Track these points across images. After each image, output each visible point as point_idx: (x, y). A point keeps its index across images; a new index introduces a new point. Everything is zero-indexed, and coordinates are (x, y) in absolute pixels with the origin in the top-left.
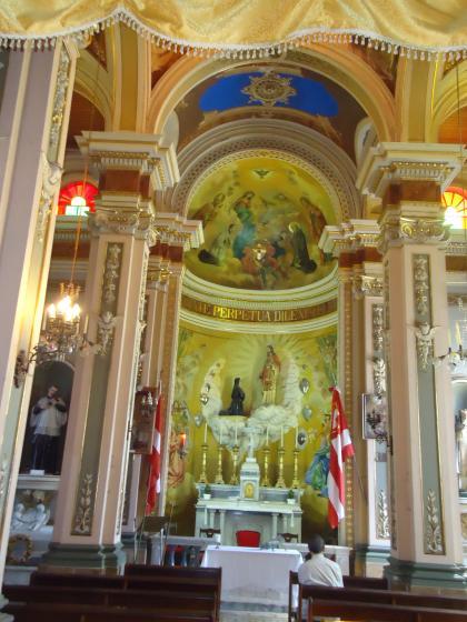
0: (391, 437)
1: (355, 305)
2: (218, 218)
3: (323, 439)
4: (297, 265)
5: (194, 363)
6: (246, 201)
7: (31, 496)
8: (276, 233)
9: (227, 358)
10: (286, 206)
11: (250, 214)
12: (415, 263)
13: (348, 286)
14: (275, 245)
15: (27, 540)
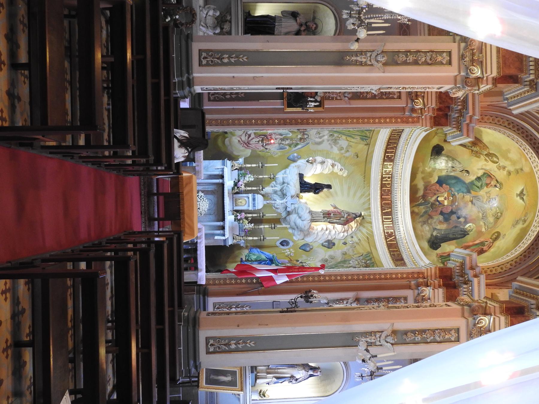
0: (295, 311)
1: (404, 282)
2: (474, 159)
3: (286, 260)
4: (435, 234)
5: (341, 149)
6: (493, 183)
7: (226, 21)
8: (464, 212)
9: (348, 176)
10: (491, 219)
12: (451, 330)
13: (420, 274)
14: (452, 213)
15: (193, 21)
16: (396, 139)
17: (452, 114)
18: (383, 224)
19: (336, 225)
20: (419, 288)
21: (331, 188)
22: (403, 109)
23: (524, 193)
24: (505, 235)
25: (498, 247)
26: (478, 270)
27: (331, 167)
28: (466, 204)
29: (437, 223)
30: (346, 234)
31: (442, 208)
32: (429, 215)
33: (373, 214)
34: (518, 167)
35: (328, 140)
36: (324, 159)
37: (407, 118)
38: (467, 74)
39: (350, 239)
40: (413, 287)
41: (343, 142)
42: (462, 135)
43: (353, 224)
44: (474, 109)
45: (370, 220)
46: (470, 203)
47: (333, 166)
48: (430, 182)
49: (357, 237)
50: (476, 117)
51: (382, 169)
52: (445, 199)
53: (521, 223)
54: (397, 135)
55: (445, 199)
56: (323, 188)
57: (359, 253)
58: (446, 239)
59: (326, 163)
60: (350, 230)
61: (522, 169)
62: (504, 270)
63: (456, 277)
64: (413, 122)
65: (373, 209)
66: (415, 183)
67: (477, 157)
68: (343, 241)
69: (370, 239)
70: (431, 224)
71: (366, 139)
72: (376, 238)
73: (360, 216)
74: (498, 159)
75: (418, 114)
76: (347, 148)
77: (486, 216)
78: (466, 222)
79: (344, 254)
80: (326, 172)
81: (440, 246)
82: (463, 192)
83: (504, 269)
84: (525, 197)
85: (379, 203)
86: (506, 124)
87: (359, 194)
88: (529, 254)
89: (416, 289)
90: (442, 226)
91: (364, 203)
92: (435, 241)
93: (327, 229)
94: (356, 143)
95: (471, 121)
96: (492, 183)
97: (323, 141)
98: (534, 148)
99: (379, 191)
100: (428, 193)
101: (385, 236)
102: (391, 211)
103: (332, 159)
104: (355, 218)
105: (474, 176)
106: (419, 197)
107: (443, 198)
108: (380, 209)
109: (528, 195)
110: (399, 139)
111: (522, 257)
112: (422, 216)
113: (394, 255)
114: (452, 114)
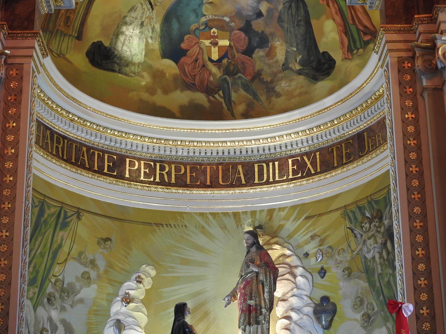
5: (86, 278)
9: (155, 264)
14: (247, 29)
16: (70, 147)
18: (275, 182)
19: (278, 294)
20: (439, 66)
21: (184, 305)
27: (132, 305)
30: (299, 271)
31: (238, 51)
33: (250, 207)
35: (63, 309)
36: (111, 323)
39: (312, 260)
40: (436, 81)
41: (71, 272)
43: (276, 252)
45: (265, 214)
47: (127, 300)
48: (175, 78)
49: (307, 243)
51: (142, 182)
52: (215, 44)
55: (215, 44)
56: (185, 325)
57: (347, 238)
59: (120, 317)
60: (288, 260)
64: (20, 78)
65: (239, 207)
66: (176, 111)
68: (317, 277)
69: (310, 212)
70: (274, 75)
71: (66, 217)
72: (307, 198)
73: (254, 234)
76: (84, 264)
79: (349, 273)
80: (142, 317)
81: (324, 53)
85: (223, 192)
87: (201, 240)
89: (442, 75)
91: (224, 227)
93: (288, 318)
94: (73, 241)
97: (63, 322)
99: (195, 192)
101: (302, 177)
102: (243, 165)
103: (110, 302)
104: (260, 248)
106: (209, 101)
108: (238, 191)
110: (69, 140)
112: (255, 96)
113: (348, 156)
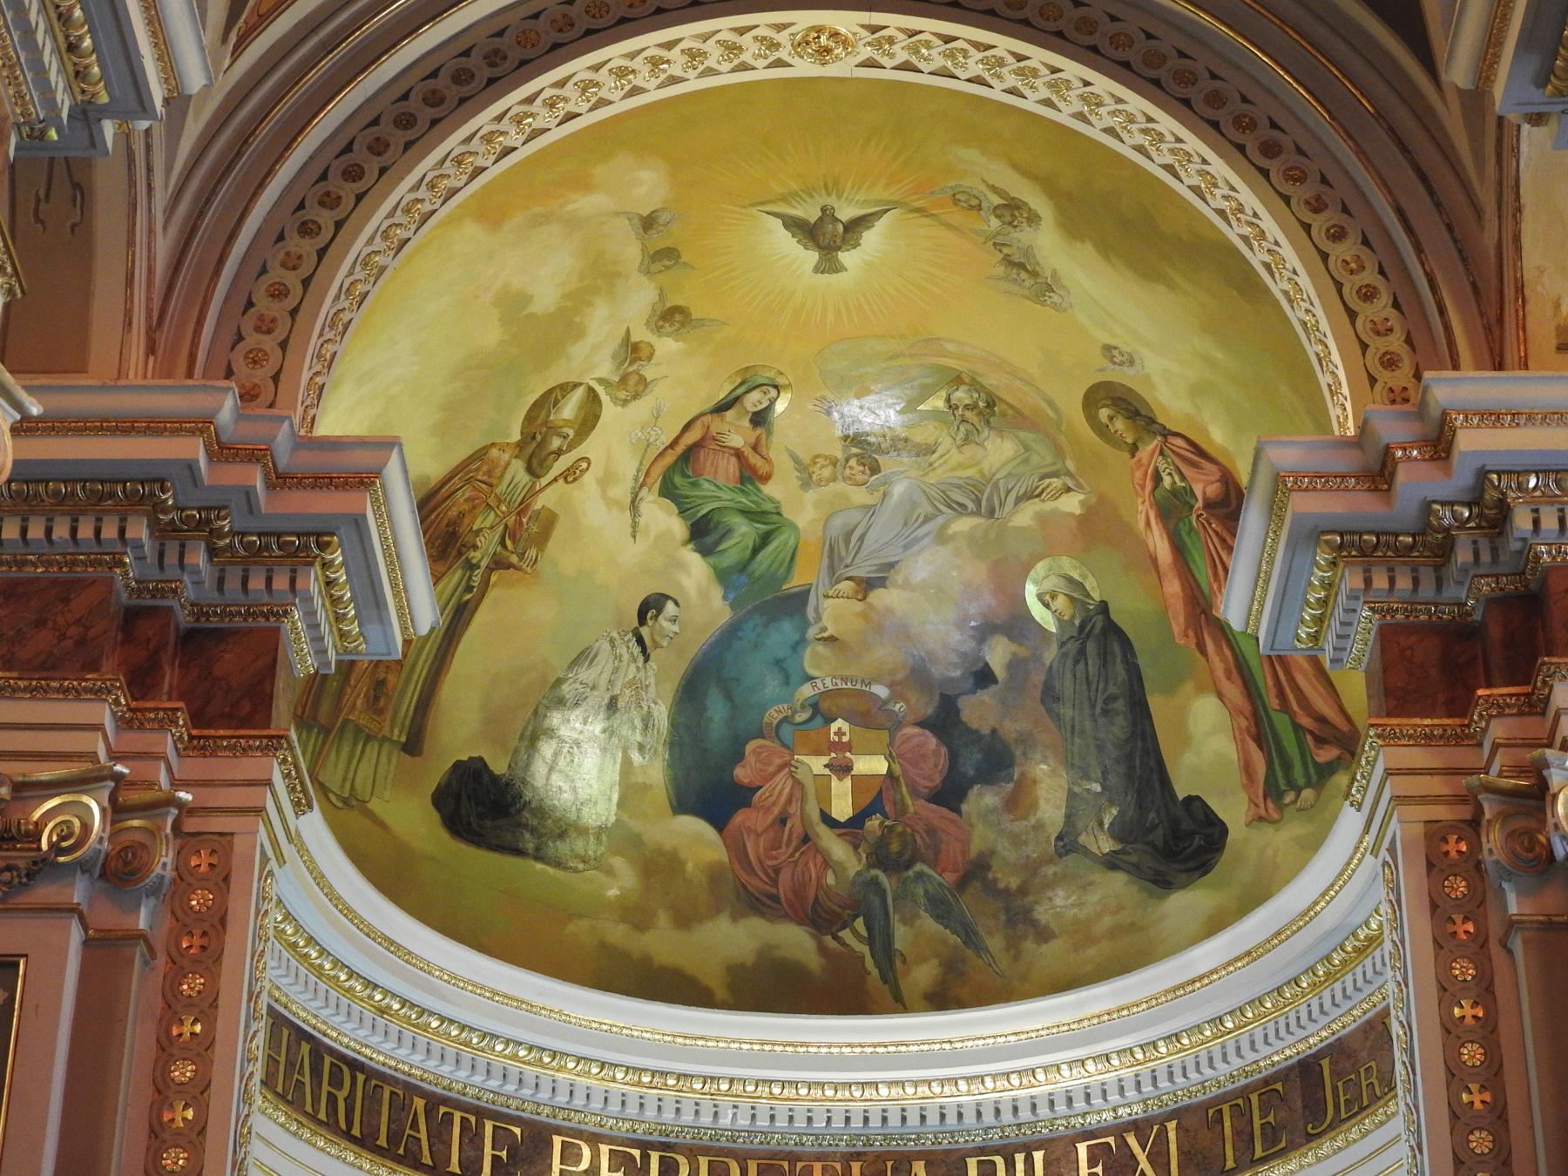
2: (560, 555)
10: (998, 452)
11: (769, 523)
14: (945, 721)
16: (372, 1098)
17: (190, 592)
22: (106, 949)
23: (811, 214)
24: (1108, 349)
25: (1198, 391)
26: (1393, 429)
28: (877, 625)
29: (1019, 826)
31: (915, 793)
32: (963, 883)
34: (631, 250)
37: (183, 920)
38: (83, 866)
42: (359, 523)
44: (155, 426)
46: (878, 597)
48: (715, 875)
50: (227, 409)
52: (843, 769)
53: (1024, 235)
54: (336, 1082)
55: (843, 769)
58: (1142, 760)
61: (648, 223)
62: (1378, 282)
63: (1452, 592)
64: (222, 880)
67: (542, 539)
70: (1031, 868)
74: (566, 388)
75: (152, 833)
77: (975, 489)
78: (1017, 624)
81: (1191, 800)
82: (799, 644)
83: (1369, 277)
84: (846, 213)
86: (308, 247)
88: (1253, 125)
90: (1042, 792)
92: (1158, 836)
95: (255, 455)
96: (736, 441)
98: (491, 81)
100: (799, 891)
105: (681, 565)
106: (823, 950)
107: (838, 779)
109: (833, 186)
110: (371, 1073)
111: (1274, 166)
112: (970, 936)
114: (190, 592)
